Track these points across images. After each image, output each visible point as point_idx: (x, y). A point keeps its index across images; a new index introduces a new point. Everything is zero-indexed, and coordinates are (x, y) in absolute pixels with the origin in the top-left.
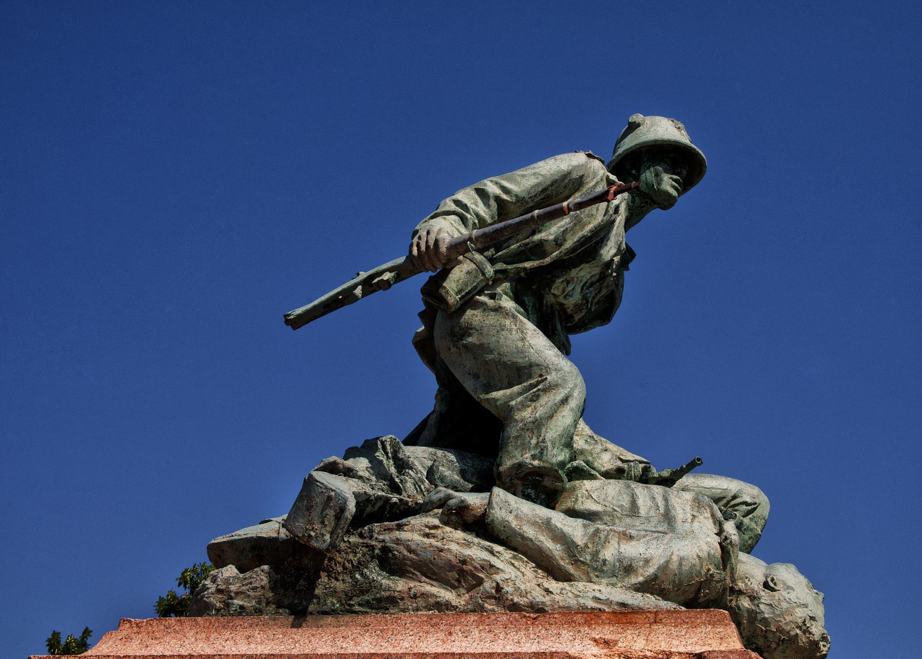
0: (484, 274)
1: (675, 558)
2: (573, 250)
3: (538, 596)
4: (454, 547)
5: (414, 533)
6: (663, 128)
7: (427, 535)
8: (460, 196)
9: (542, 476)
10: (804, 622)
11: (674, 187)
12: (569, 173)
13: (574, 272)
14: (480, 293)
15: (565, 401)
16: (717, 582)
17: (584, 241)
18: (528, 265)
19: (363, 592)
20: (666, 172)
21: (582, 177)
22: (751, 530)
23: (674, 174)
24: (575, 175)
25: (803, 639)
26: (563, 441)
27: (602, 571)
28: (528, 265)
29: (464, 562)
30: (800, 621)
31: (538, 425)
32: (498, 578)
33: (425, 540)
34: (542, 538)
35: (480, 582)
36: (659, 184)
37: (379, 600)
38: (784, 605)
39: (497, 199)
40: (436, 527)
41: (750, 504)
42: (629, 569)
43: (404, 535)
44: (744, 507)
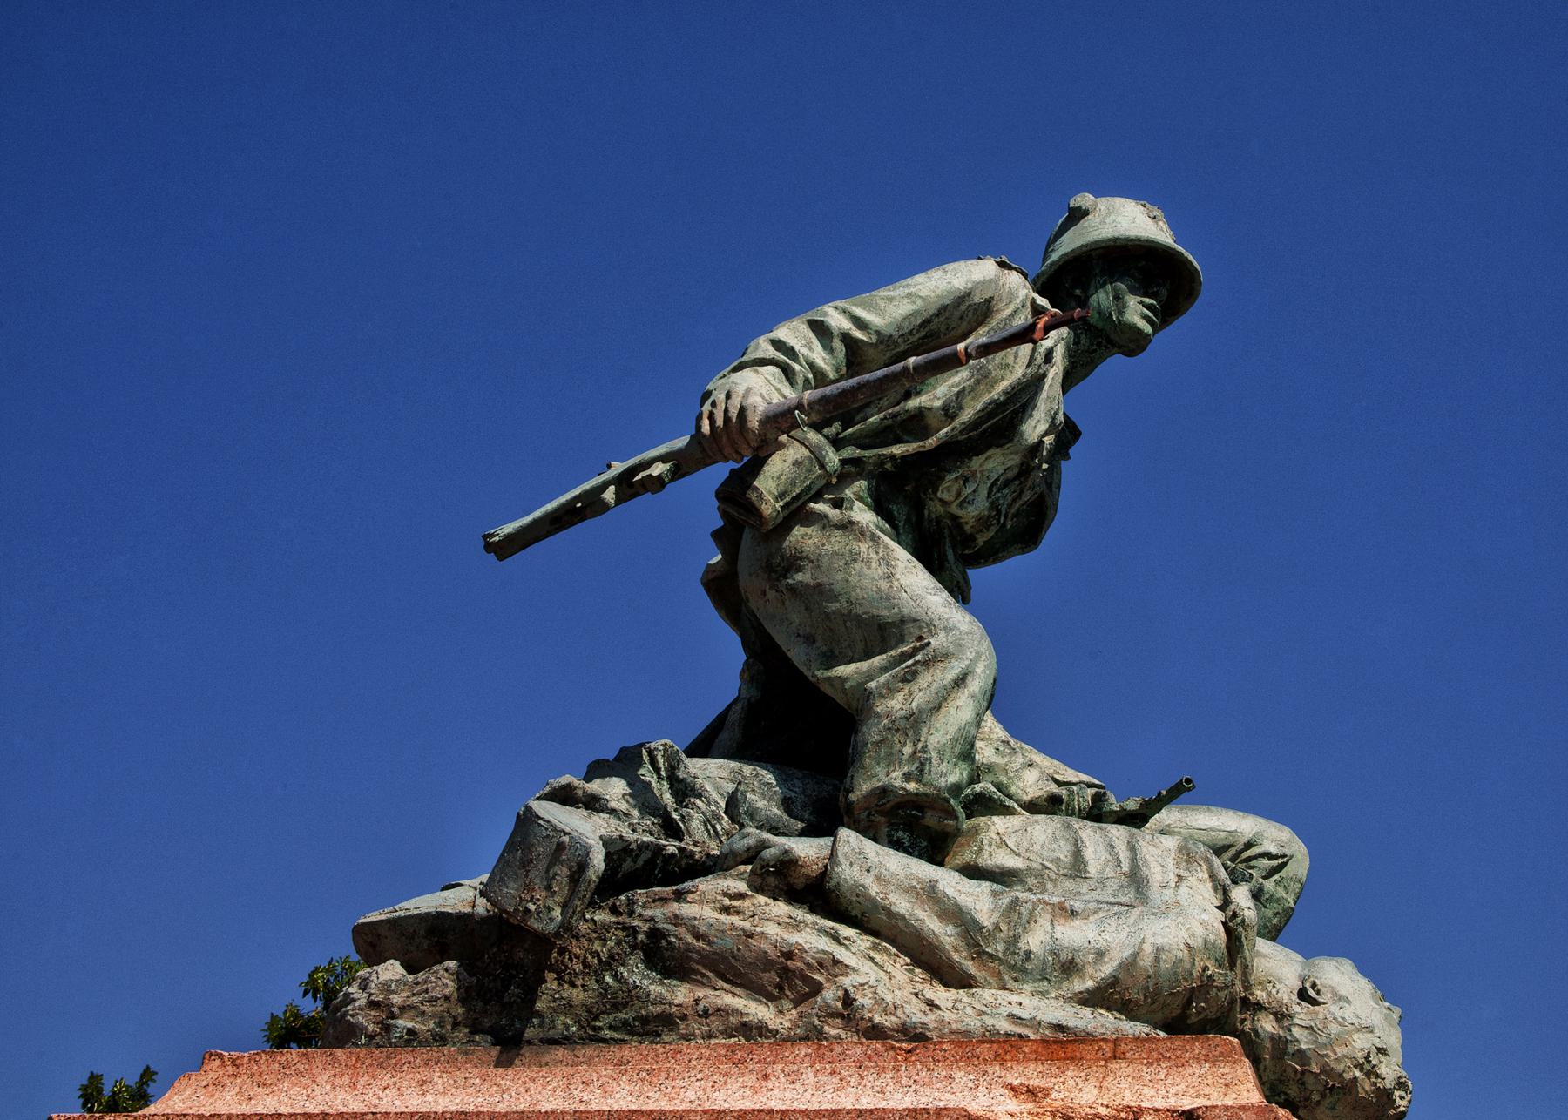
0: (822, 466)
1: (1148, 948)
2: (974, 424)
3: (915, 1013)
4: (772, 930)
5: (704, 907)
6: (1126, 218)
7: (726, 910)
8: (782, 333)
9: (921, 808)
10: (1367, 1058)
11: (1145, 318)
12: (968, 294)
13: (976, 463)
14: (817, 497)
15: (960, 681)
16: (1220, 989)
17: (994, 409)
18: (897, 450)
19: (617, 1006)
20: (1133, 292)
21: (990, 300)
22: (1278, 901)
23: (1146, 295)
24: (977, 298)
25: (1366, 1086)
26: (957, 750)
27: (1024, 971)
28: (897, 450)
29: (789, 955)
30: (1360, 1055)
31: (914, 722)
32: (847, 981)
33: (724, 918)
34: (921, 914)
35: (817, 989)
36: (1121, 312)
37: (645, 1020)
38: (1334, 1028)
39: (846, 338)
40: (741, 896)
41: (1275, 857)
42: (1069, 968)
43: (688, 910)
44: (1266, 862)
